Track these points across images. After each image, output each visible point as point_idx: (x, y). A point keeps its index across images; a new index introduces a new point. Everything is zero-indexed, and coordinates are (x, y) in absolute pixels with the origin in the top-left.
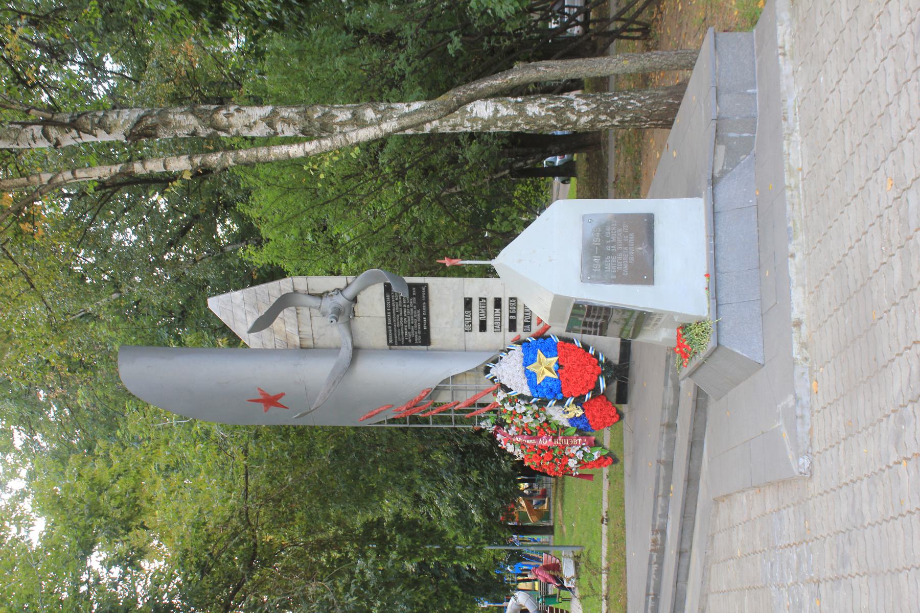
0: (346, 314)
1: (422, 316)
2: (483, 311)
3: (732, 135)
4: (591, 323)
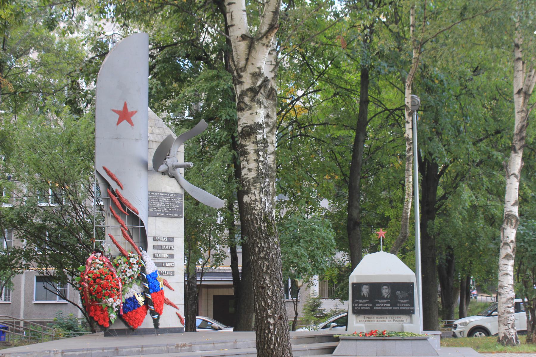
2: (167, 248)
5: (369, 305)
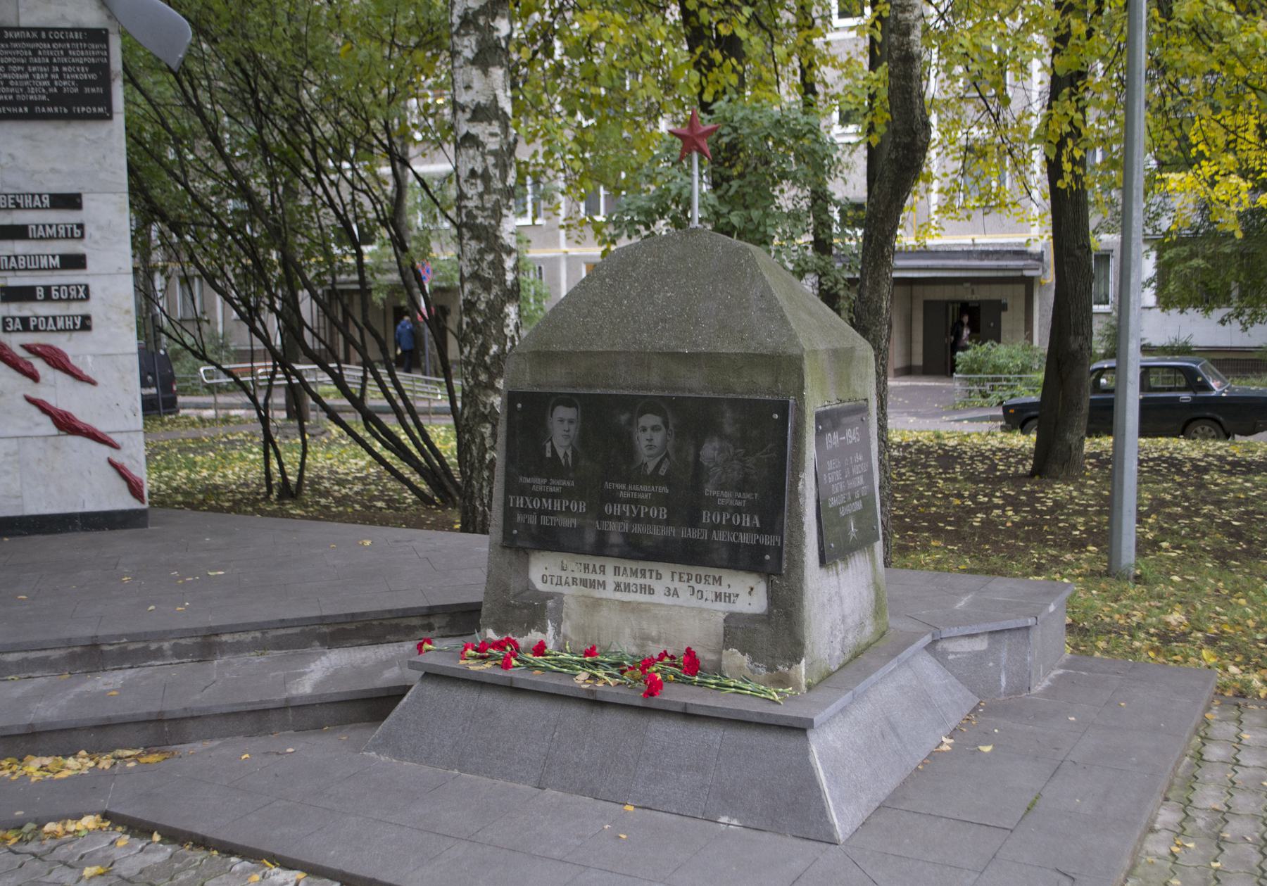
1: (31, 104)
2: (53, 232)
5: (574, 506)
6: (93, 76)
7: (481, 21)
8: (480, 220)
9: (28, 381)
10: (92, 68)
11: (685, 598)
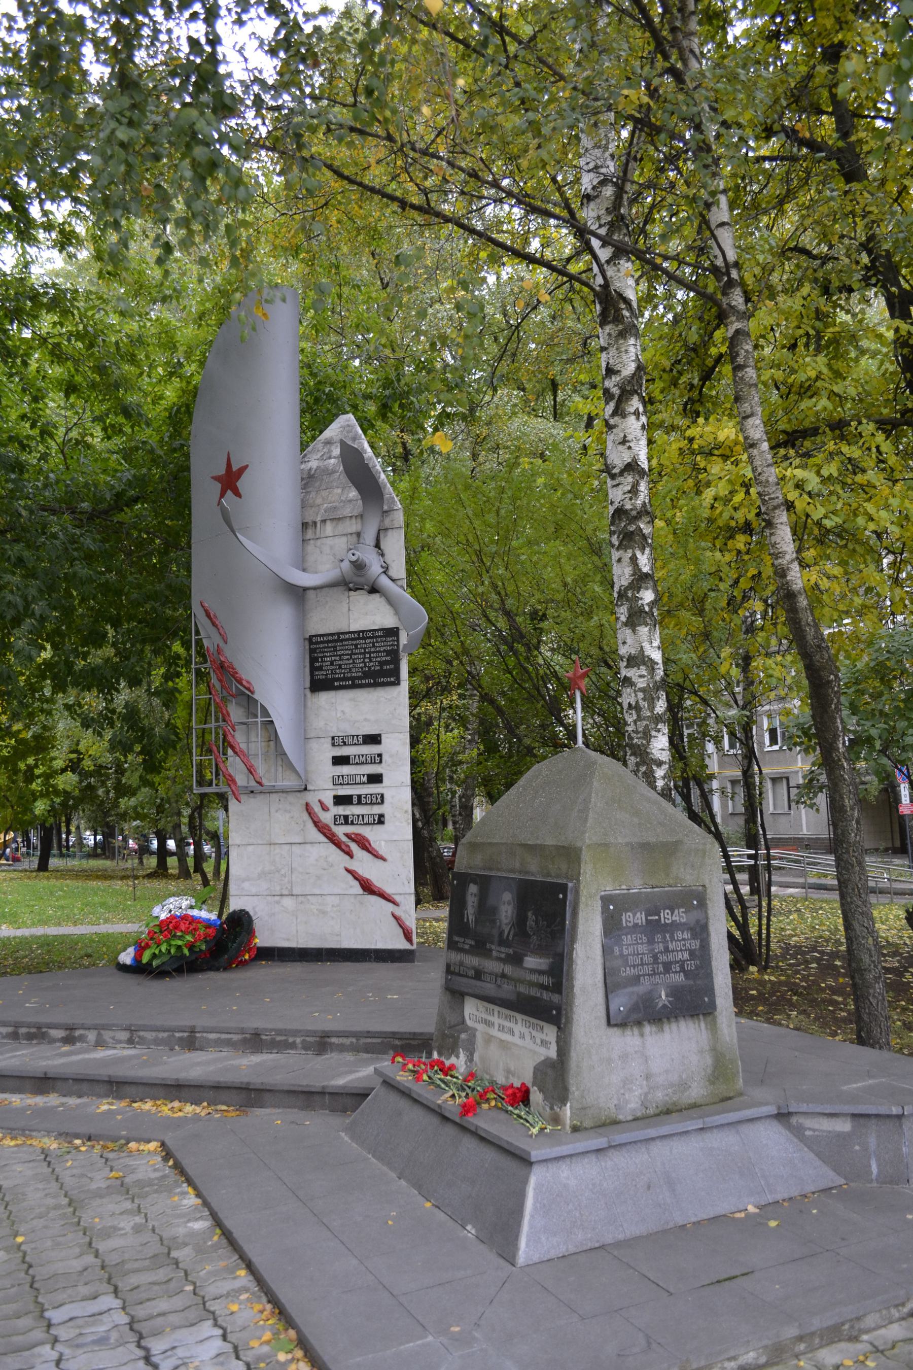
0: (356, 579)
2: (363, 759)
3: (872, 1141)
4: (96, 894)
6: (388, 658)
7: (630, 595)
8: (635, 741)
9: (347, 857)
10: (388, 653)
11: (528, 1043)
